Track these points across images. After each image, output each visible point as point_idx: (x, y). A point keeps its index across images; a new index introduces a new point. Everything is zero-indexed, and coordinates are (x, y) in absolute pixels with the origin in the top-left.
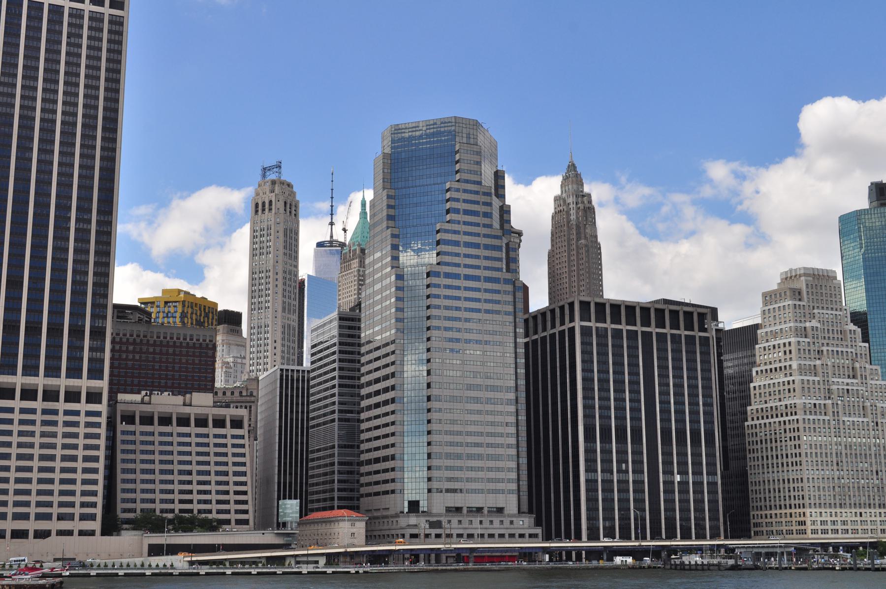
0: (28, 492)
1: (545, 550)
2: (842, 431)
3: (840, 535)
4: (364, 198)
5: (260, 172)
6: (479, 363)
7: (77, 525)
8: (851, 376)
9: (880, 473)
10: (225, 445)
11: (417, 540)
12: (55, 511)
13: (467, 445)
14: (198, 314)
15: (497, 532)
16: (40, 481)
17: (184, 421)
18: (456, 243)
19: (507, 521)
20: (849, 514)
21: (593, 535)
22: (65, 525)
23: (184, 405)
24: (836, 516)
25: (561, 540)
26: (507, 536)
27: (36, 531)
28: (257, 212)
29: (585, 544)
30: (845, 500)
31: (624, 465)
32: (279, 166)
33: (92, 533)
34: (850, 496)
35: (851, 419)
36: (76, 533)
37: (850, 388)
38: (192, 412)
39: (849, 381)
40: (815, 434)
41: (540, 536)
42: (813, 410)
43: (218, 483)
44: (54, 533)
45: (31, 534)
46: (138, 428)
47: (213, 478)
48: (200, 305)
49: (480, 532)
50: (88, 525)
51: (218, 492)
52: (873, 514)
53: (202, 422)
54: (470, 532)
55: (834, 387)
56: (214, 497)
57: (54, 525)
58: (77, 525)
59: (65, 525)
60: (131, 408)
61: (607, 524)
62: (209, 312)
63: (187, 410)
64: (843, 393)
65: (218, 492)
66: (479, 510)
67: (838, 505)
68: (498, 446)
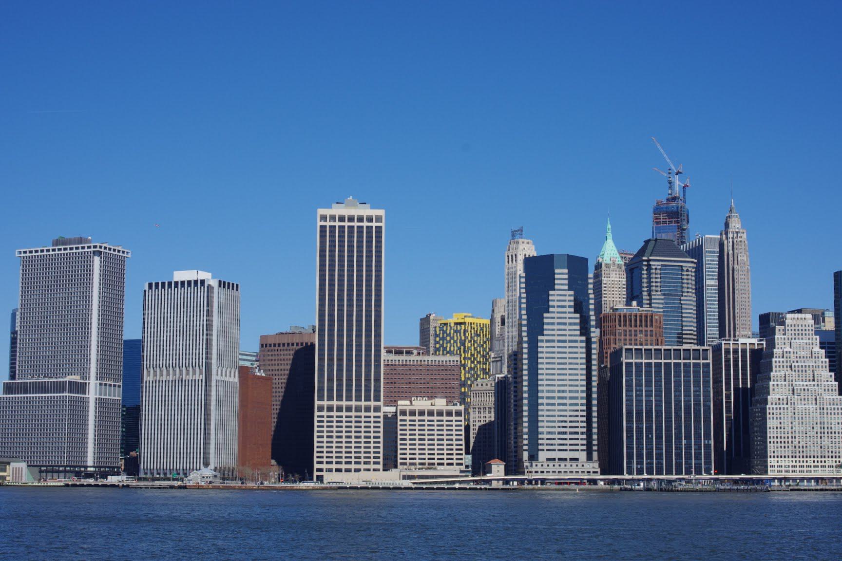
0: (346, 452)
1: (602, 480)
3: (776, 473)
5: (510, 234)
7: (372, 466)
10: (452, 426)
12: (353, 460)
14: (476, 329)
15: (574, 470)
16: (337, 452)
17: (431, 413)
18: (553, 324)
19: (539, 465)
21: (630, 472)
22: (367, 466)
23: (432, 405)
26: (580, 472)
27: (345, 469)
28: (516, 255)
29: (627, 476)
31: (650, 436)
32: (522, 230)
33: (379, 470)
36: (372, 470)
38: (435, 408)
41: (599, 472)
42: (778, 402)
43: (448, 445)
44: (362, 470)
45: (353, 470)
46: (408, 418)
47: (445, 442)
48: (477, 323)
50: (376, 467)
51: (447, 449)
53: (440, 414)
56: (427, 456)
57: (343, 466)
58: (372, 466)
59: (367, 466)
60: (404, 408)
61: (687, 466)
62: (483, 327)
63: (432, 408)
65: (447, 449)
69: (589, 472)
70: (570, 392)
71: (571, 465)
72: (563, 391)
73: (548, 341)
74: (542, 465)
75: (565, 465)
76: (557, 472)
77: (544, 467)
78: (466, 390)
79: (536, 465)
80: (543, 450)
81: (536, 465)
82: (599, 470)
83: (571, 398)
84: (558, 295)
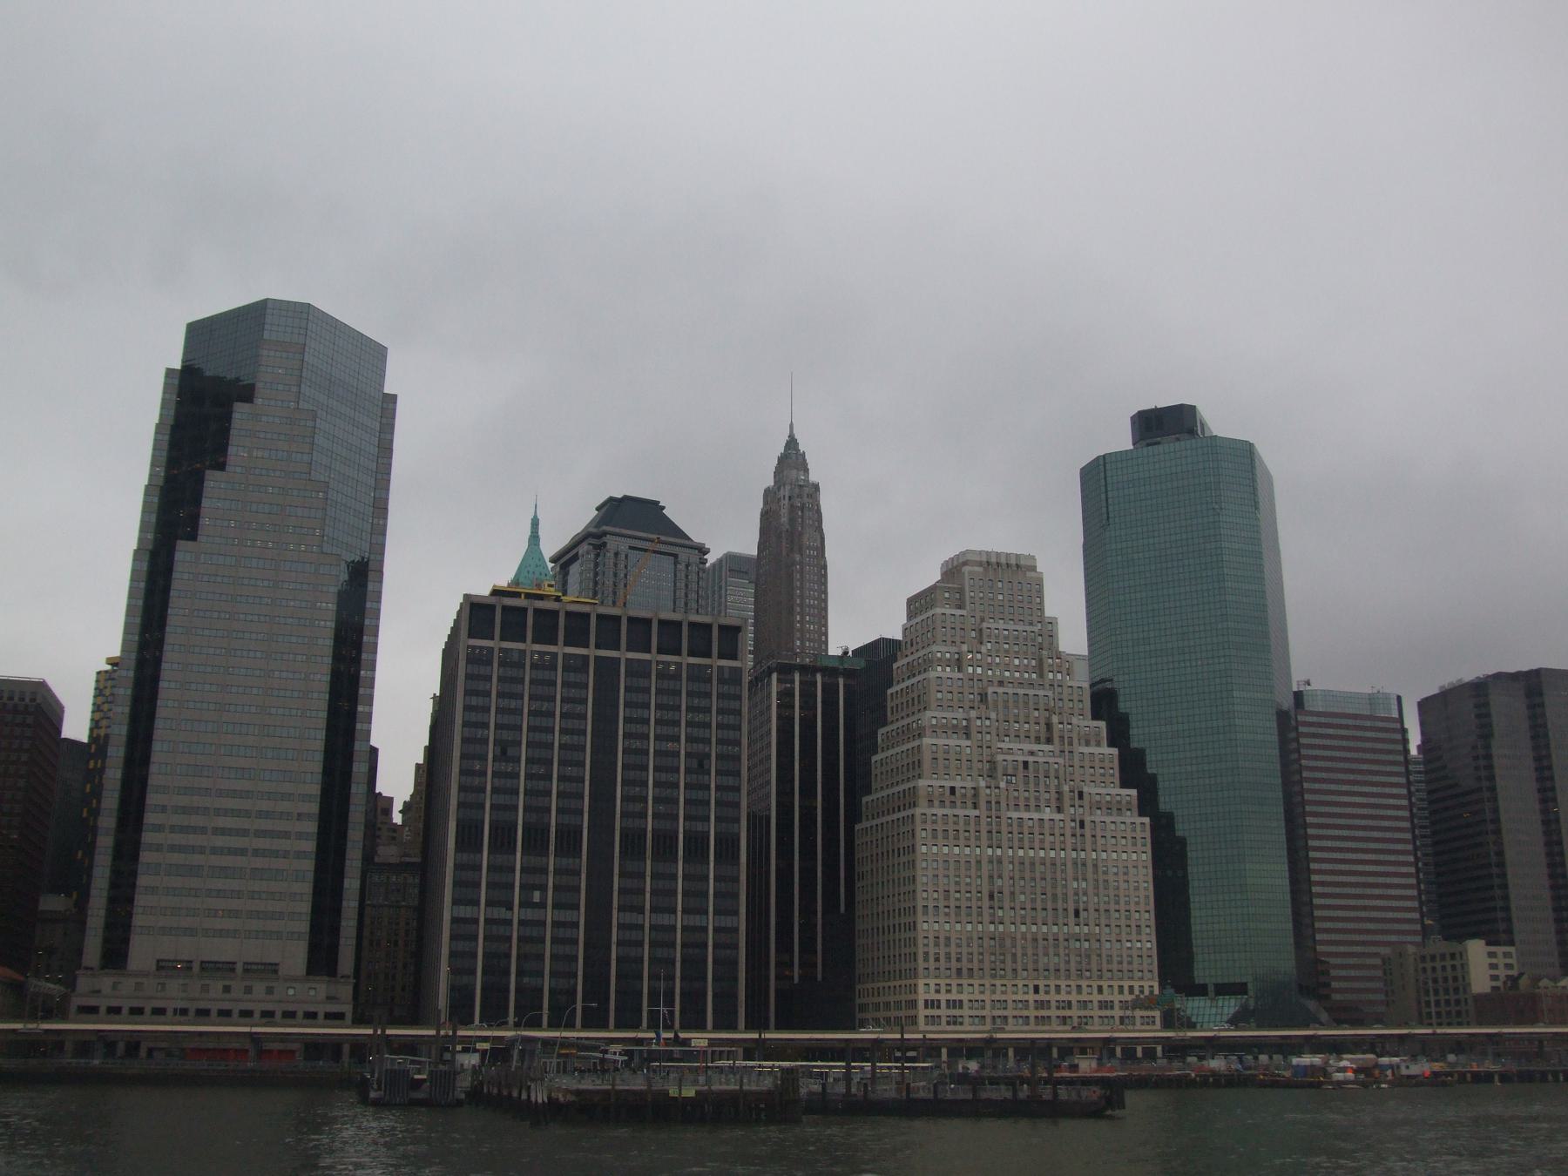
2: (1005, 836)
4: (535, 516)
6: (253, 709)
8: (1043, 739)
9: (1083, 914)
11: (162, 1018)
13: (215, 851)
20: (1010, 989)
24: (1047, 992)
25: (854, 1029)
30: (1003, 962)
34: (1014, 955)
35: (1036, 816)
37: (1031, 759)
39: (1035, 747)
40: (1134, 849)
49: (181, 1005)
52: (932, 987)
54: (203, 1005)
55: (1000, 758)
64: (1016, 769)
66: (230, 967)
67: (987, 971)
68: (192, 849)
82: (347, 1009)
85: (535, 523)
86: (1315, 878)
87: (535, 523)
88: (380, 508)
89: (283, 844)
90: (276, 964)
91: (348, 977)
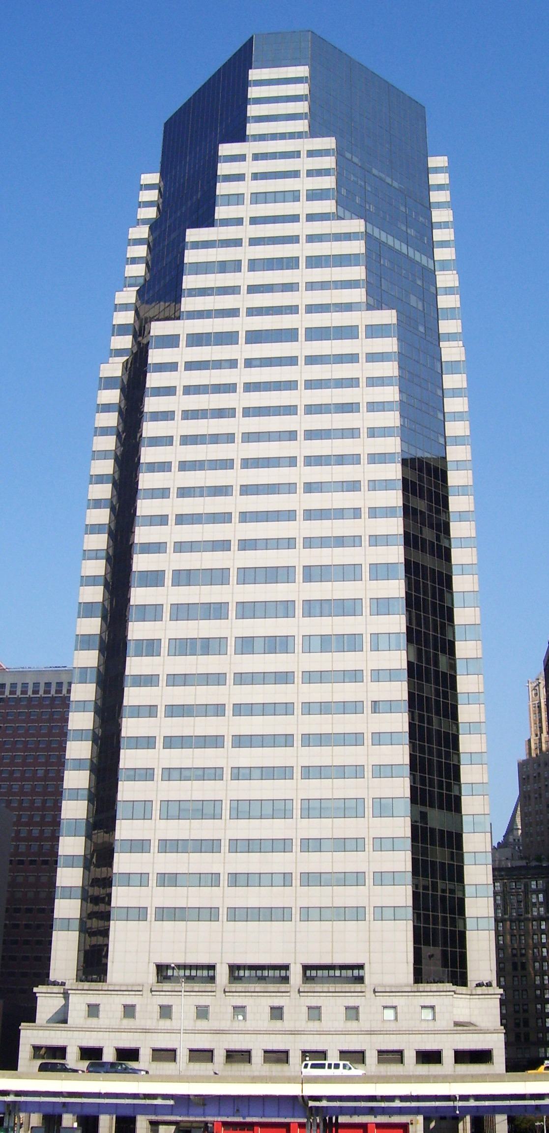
15: (183, 1045)
54: (238, 1043)
69: (430, 1057)
70: (311, 574)
71: (315, 1012)
72: (326, 643)
73: (196, 340)
74: (129, 1011)
75: (277, 1013)
76: (220, 1056)
77: (287, 1023)
78: (538, 978)
79: (93, 1010)
80: (140, 914)
81: (93, 1010)
82: (496, 1043)
83: (314, 608)
84: (256, 157)
85: (491, 824)
86: (302, 89)
87: (491, 824)
88: (462, 823)
89: (277, 862)
90: (361, 967)
91: (489, 985)
